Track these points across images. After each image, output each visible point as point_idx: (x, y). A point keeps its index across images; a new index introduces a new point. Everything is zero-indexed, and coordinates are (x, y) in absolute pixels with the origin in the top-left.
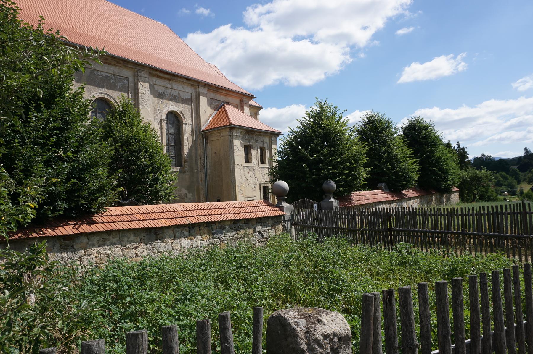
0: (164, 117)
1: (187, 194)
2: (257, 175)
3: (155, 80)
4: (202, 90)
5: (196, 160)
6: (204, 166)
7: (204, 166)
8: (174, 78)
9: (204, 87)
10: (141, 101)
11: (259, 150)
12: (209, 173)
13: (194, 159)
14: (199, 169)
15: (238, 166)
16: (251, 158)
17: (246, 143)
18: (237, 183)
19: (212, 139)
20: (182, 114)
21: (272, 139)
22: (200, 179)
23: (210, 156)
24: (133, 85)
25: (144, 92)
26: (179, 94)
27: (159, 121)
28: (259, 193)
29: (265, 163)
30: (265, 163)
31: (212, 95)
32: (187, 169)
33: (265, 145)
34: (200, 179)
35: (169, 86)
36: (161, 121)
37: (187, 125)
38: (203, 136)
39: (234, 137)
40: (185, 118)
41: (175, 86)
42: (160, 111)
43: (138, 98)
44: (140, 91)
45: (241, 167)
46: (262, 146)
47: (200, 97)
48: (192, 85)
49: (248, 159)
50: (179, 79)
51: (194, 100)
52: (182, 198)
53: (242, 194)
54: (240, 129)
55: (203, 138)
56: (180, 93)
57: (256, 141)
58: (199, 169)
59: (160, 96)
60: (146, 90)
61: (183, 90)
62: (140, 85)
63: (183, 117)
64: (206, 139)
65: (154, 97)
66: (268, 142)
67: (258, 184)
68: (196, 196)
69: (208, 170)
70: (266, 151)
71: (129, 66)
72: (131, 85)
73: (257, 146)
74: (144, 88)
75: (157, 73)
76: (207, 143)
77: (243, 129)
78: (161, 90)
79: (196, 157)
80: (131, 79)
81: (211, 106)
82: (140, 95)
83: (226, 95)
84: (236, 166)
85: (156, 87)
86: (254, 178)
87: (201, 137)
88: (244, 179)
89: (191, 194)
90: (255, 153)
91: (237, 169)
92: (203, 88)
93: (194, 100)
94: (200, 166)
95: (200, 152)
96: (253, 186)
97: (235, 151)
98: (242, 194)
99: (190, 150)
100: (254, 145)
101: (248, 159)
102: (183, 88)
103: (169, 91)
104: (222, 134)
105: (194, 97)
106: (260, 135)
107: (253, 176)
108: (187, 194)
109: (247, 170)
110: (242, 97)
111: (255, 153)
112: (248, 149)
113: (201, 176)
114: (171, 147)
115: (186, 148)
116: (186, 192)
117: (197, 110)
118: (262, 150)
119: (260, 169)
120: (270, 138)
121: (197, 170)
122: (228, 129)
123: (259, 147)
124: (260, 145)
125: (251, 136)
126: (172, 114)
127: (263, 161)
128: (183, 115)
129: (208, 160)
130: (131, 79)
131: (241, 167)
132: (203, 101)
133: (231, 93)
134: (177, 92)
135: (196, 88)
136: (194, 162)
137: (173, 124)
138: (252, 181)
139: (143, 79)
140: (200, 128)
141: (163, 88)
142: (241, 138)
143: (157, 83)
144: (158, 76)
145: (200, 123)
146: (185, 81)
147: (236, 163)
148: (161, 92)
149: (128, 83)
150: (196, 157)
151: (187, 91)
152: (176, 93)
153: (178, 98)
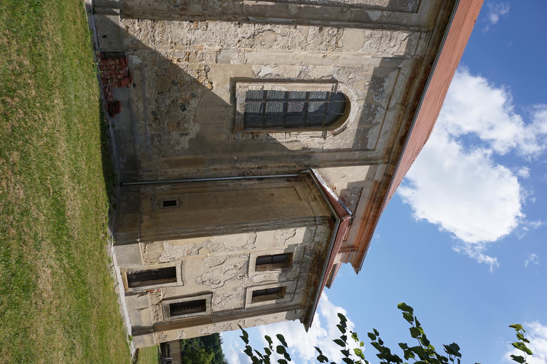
0: (341, 88)
1: (188, 138)
2: (230, 285)
3: (406, 70)
4: (381, 169)
5: (256, 157)
6: (245, 175)
7: (245, 175)
8: (408, 110)
9: (386, 175)
10: (378, 33)
11: (275, 286)
12: (231, 184)
13: (258, 154)
14: (238, 165)
15: (252, 241)
16: (264, 269)
17: (294, 257)
18: (215, 239)
19: (298, 188)
20: (343, 130)
21: (299, 311)
22: (218, 167)
23: (265, 185)
24: (405, 22)
25: (392, 44)
26: (377, 124)
27: (335, 76)
28: (196, 291)
29: (253, 301)
30: (253, 301)
31: (367, 192)
32: (240, 137)
33: (287, 298)
34: (218, 167)
35: (393, 102)
36: (334, 81)
37: (322, 140)
38: (301, 172)
39: (313, 228)
40: (335, 135)
41: (391, 116)
42: (352, 82)
43: (383, 28)
44: (396, 33)
45: (250, 247)
46: (287, 290)
47: (368, 167)
48: (389, 151)
49: (264, 262)
50: (404, 122)
51: (364, 155)
52: (178, 124)
53: (189, 254)
54: (328, 242)
55: (299, 172)
56: (379, 127)
57: (297, 278)
58: (238, 165)
59: (377, 82)
60: (396, 48)
61: (383, 132)
62: (406, 35)
63: (336, 130)
64: (296, 179)
65: (376, 70)
66: (292, 303)
67: (212, 288)
68: (182, 157)
69: (237, 183)
70: (274, 302)
71: (441, 12)
72: (405, 19)
73: (288, 280)
74: (396, 44)
75: (421, 76)
76: (288, 180)
77: (327, 247)
78: (388, 84)
79: (262, 158)
80: (414, 18)
81: (348, 189)
82: (389, 33)
83: (365, 219)
84: (252, 235)
85: (393, 74)
86: (223, 278)
87: (298, 168)
88: (222, 254)
89: (187, 146)
90: (272, 277)
91: (245, 237)
92: (383, 171)
93: (364, 155)
94: (245, 166)
95: (272, 166)
96: (206, 277)
97: (284, 231)
98: (189, 254)
99: (279, 146)
100: (290, 275)
101: (264, 262)
102: (386, 132)
103: (384, 104)
104: (313, 204)
105: (369, 155)
106: (309, 285)
107: (227, 277)
108: (188, 138)
109: (240, 262)
110: (360, 248)
111: (272, 277)
112: (282, 261)
113: (225, 168)
114: (282, 104)
115: (280, 137)
116: (192, 135)
117: (347, 160)
118: (278, 292)
119: (241, 290)
120: (300, 306)
121: (236, 161)
122: (328, 214)
123: (284, 285)
124: (290, 286)
125: (308, 266)
126: (342, 104)
127: (257, 295)
128: (339, 132)
129: (257, 182)
130: (414, 18)
131: (250, 247)
132: (358, 173)
133: (368, 226)
134: (381, 121)
135: (383, 159)
136: (252, 154)
137: (324, 109)
138: (217, 274)
139: (414, 42)
140: (316, 167)
141: (390, 90)
142: (307, 244)
143: (401, 77)
144: (412, 79)
145: (325, 166)
146: (400, 134)
147: (259, 234)
148: (385, 85)
149: (408, 12)
150: (262, 158)
151: (380, 140)
152: (378, 118)
153: (371, 122)
